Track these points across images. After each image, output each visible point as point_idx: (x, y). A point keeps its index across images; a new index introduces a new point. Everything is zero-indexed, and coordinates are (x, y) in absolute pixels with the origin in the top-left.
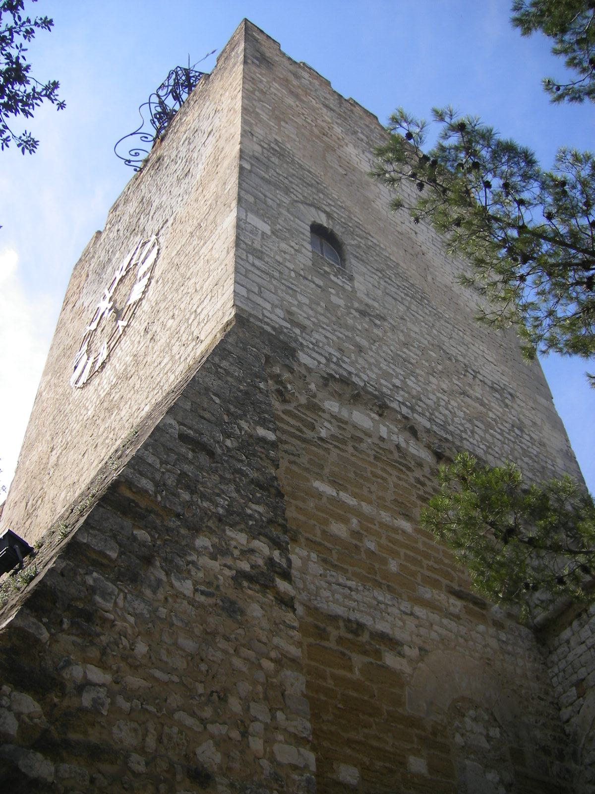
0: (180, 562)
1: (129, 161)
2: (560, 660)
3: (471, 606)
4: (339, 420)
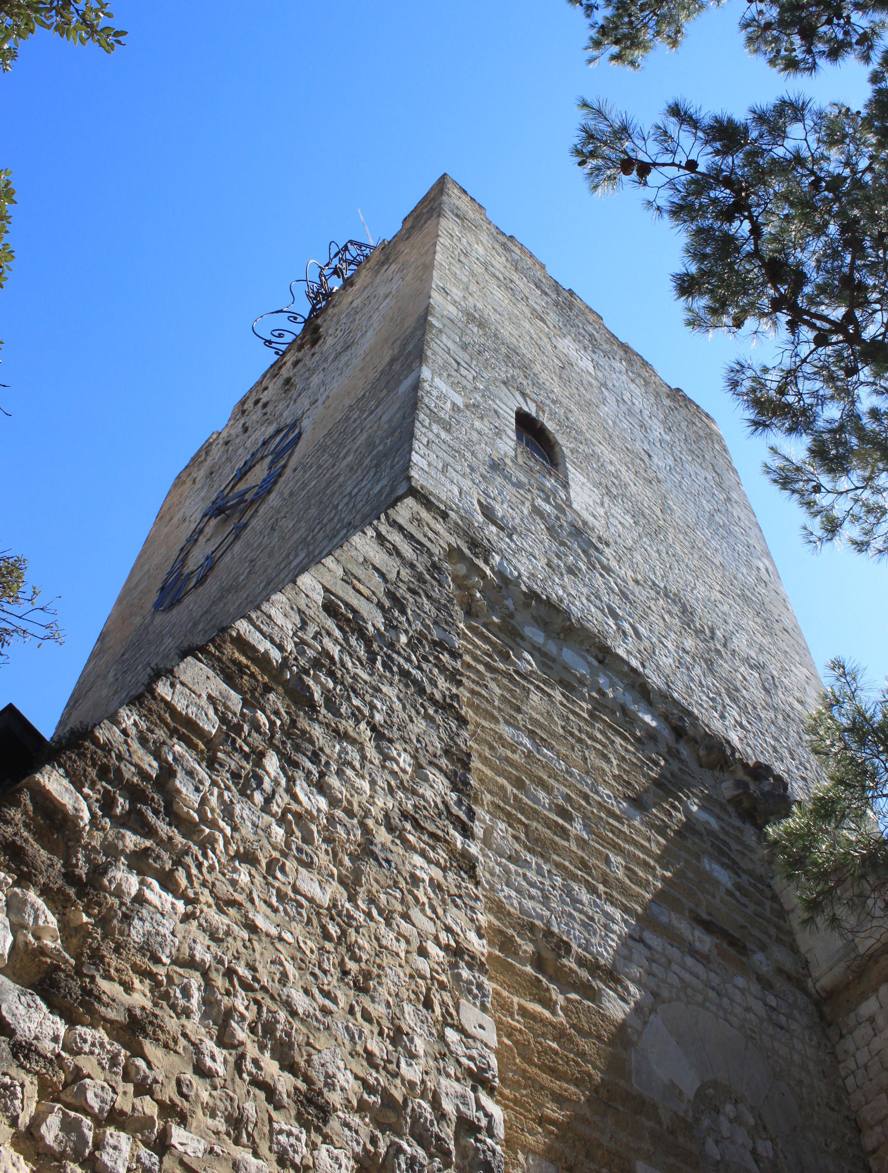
0: (236, 1114)
1: (270, 342)
2: (858, 1049)
3: (725, 946)
4: (545, 655)
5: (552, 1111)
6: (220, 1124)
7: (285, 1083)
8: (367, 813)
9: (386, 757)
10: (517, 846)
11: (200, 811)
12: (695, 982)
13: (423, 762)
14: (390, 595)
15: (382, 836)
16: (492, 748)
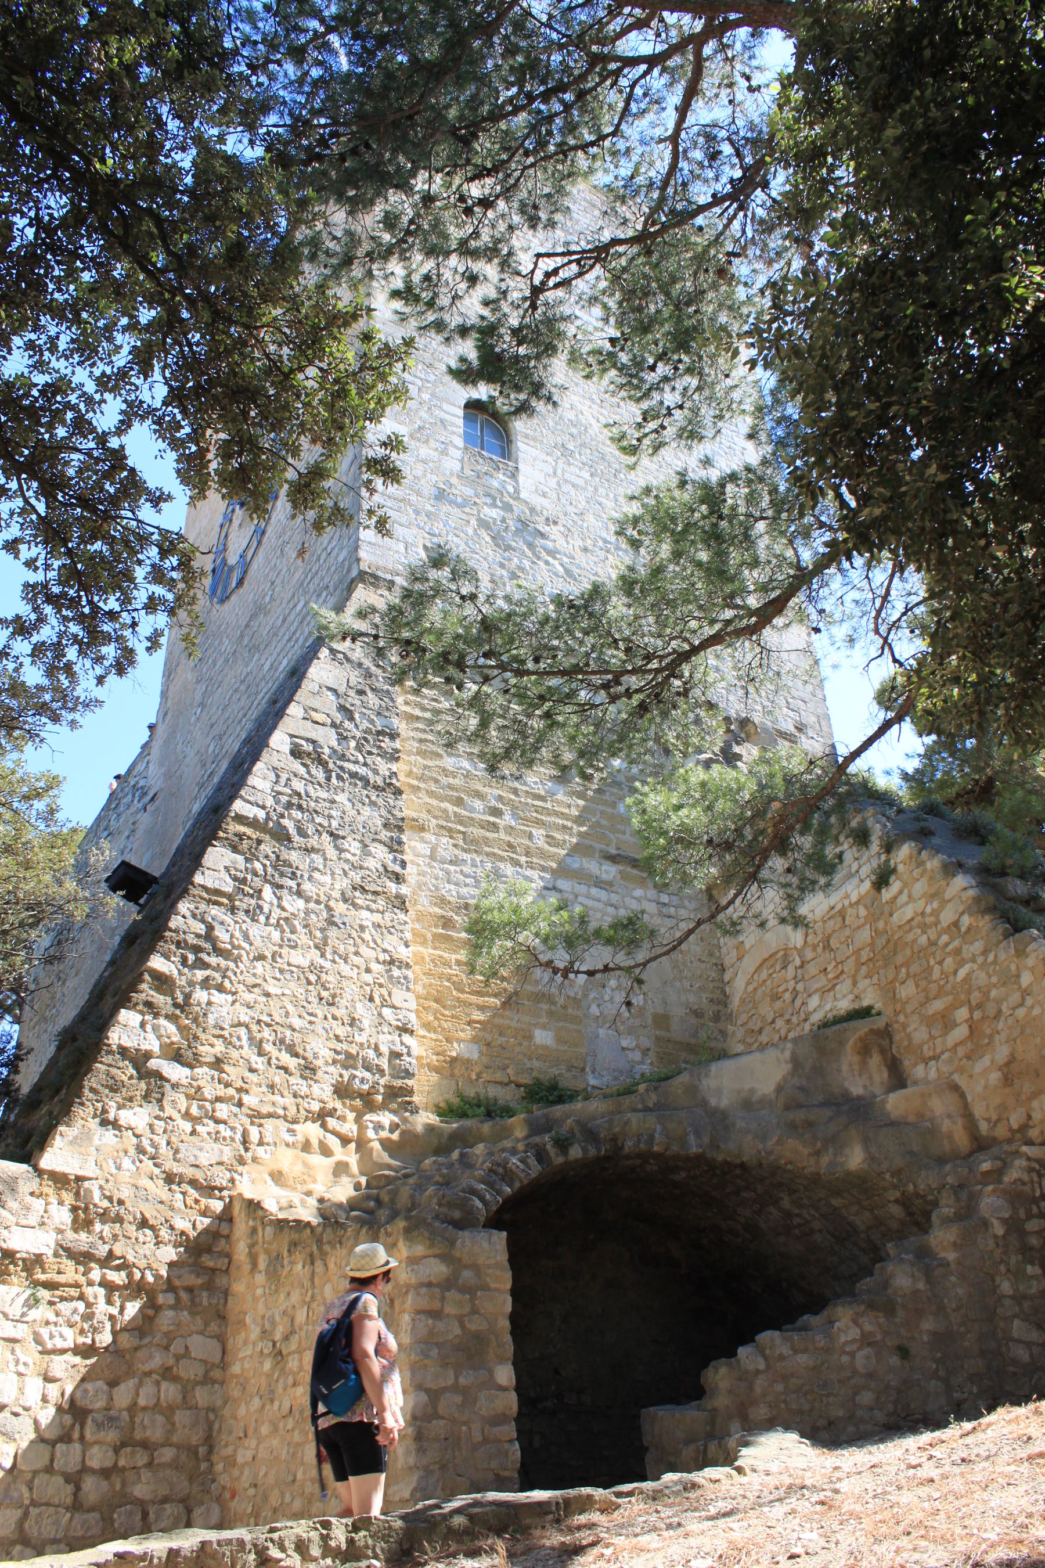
5: (477, 1016)
6: (264, 1089)
7: (292, 1063)
8: (329, 898)
9: (341, 851)
10: (456, 852)
11: (231, 943)
12: (596, 904)
13: (368, 841)
14: (342, 708)
15: (340, 908)
16: (436, 781)
